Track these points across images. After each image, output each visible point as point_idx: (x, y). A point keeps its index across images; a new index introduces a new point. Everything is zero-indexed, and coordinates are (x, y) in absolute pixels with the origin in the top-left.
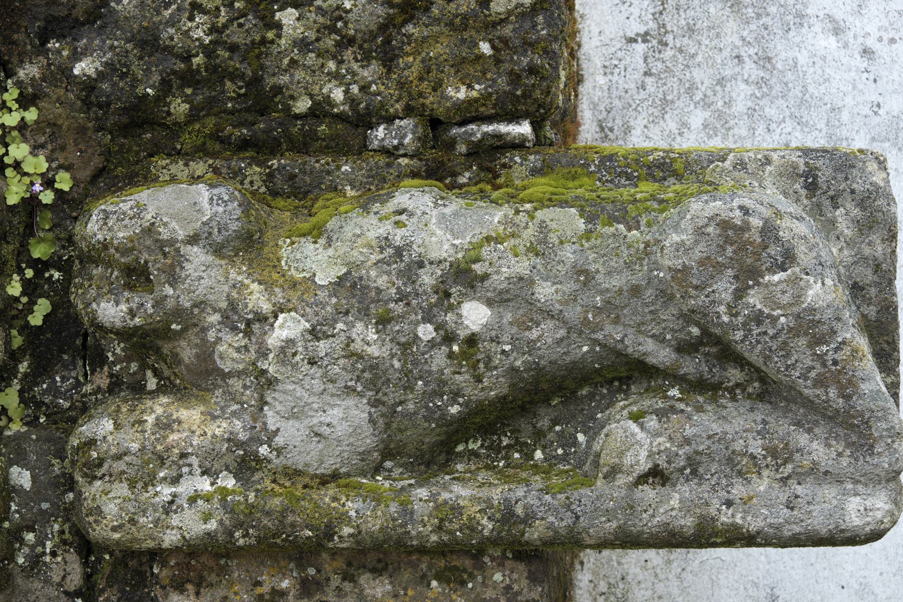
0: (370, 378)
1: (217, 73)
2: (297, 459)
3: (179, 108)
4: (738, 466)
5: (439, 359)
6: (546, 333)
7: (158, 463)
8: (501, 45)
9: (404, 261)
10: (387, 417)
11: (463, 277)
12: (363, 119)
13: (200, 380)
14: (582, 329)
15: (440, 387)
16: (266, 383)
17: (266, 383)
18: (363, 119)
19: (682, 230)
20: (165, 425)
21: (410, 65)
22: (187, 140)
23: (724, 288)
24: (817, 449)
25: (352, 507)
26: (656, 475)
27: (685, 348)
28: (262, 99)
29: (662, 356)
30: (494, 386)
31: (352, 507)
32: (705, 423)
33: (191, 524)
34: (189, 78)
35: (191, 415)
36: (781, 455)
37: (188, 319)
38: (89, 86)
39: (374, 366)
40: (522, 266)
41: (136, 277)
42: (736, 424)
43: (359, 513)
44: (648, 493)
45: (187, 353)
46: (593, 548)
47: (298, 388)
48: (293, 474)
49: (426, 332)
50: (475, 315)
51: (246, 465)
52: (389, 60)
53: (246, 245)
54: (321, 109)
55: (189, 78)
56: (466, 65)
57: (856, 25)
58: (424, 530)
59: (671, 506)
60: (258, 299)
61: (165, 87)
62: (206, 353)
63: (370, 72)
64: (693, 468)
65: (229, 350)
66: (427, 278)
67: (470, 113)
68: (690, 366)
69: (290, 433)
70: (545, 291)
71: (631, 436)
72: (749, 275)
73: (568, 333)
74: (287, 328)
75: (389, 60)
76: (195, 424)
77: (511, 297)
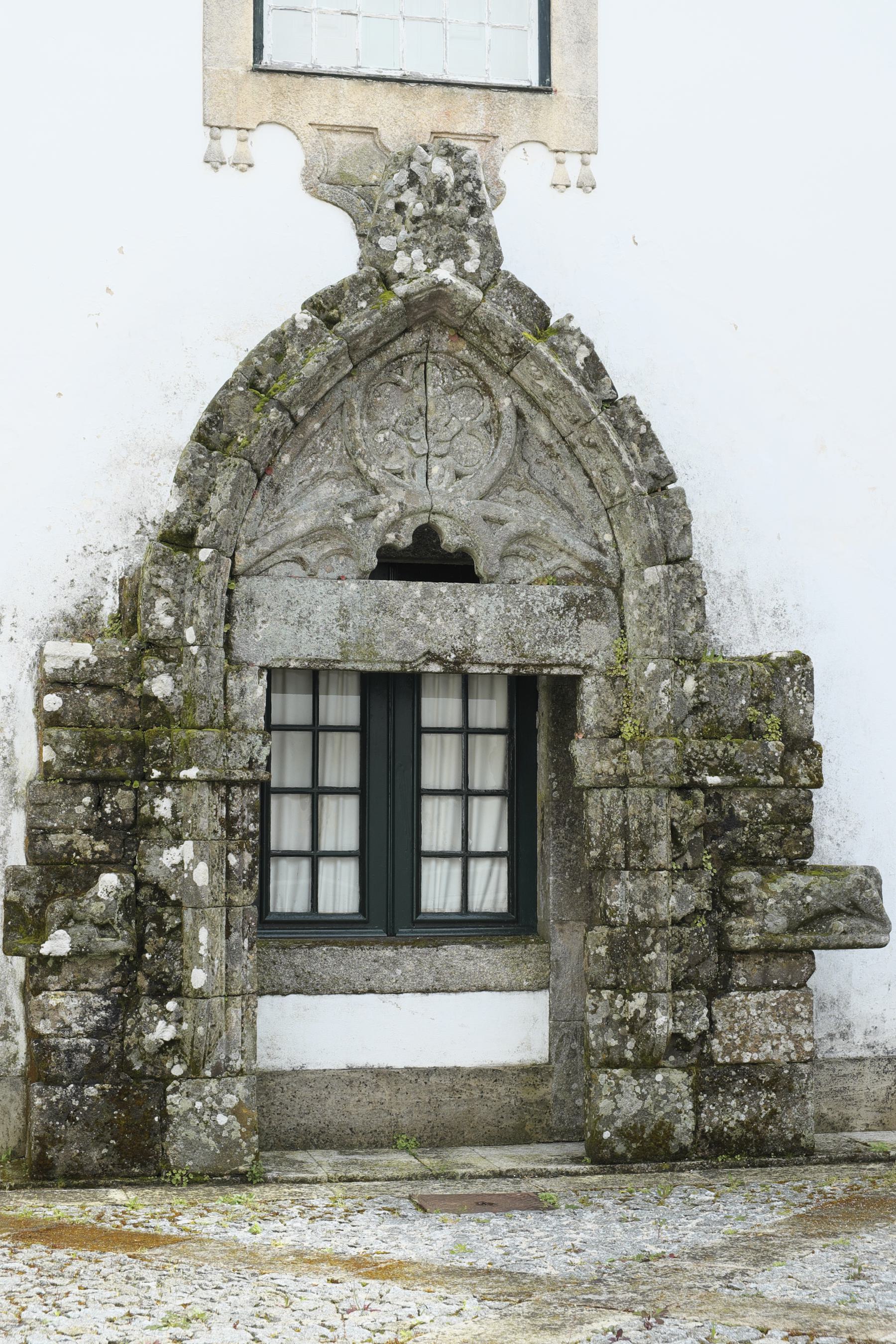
0: (788, 912)
1: (747, 848)
2: (771, 930)
3: (739, 855)
4: (860, 930)
5: (801, 908)
6: (822, 902)
7: (745, 930)
8: (804, 842)
9: (795, 887)
10: (790, 921)
11: (807, 890)
12: (775, 858)
13: (751, 913)
14: (829, 902)
15: (801, 914)
16: (766, 913)
17: (766, 913)
18: (775, 858)
19: (849, 884)
20: (746, 922)
21: (785, 847)
22: (739, 863)
23: (858, 893)
24: (875, 926)
25: (785, 939)
26: (845, 933)
27: (848, 906)
28: (756, 853)
29: (844, 908)
30: (811, 914)
31: (785, 939)
32: (854, 921)
33: (752, 944)
34: (742, 849)
35: (750, 920)
36: (869, 927)
37: (750, 899)
38: (721, 850)
39: (789, 910)
40: (819, 888)
41: (742, 891)
42: (855, 922)
43: (787, 941)
44: (843, 936)
45: (748, 907)
46: (168, 1237)
47: (774, 914)
48: (770, 933)
49: (799, 902)
50: (809, 899)
51: (762, 931)
52: (781, 845)
53: (761, 885)
54: (767, 856)
55: (742, 849)
56: (797, 847)
57: (836, 838)
58: (799, 945)
59: (848, 939)
60: (765, 895)
61: (737, 851)
62: (753, 907)
63: (777, 848)
64: (852, 931)
65: (758, 907)
66: (800, 891)
67: (797, 857)
68: (849, 910)
69: (770, 924)
70: (823, 894)
71: (840, 924)
72: (862, 890)
73: (70, 1061)
74: (771, 902)
75: (781, 845)
76: (752, 923)
77: (816, 895)
